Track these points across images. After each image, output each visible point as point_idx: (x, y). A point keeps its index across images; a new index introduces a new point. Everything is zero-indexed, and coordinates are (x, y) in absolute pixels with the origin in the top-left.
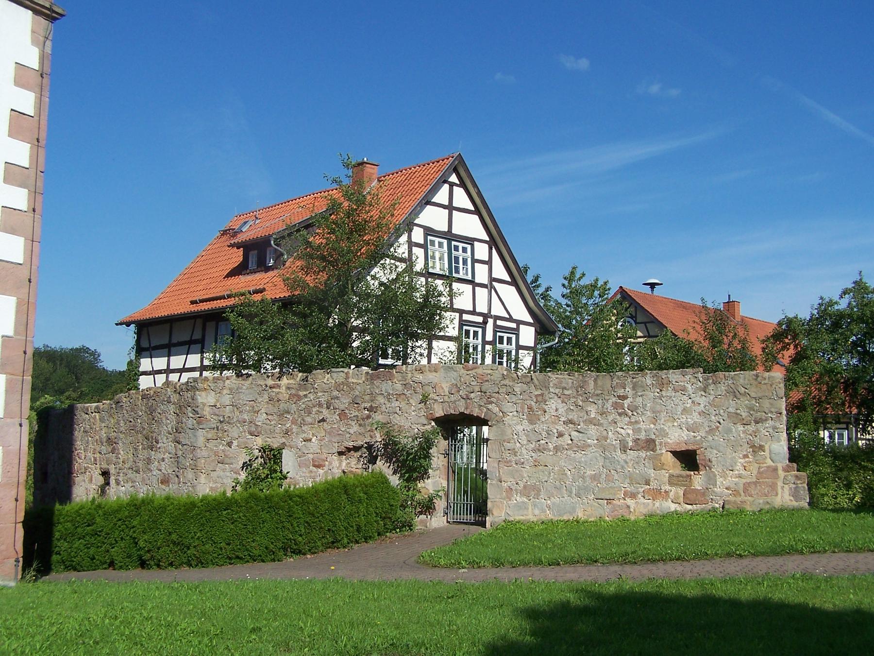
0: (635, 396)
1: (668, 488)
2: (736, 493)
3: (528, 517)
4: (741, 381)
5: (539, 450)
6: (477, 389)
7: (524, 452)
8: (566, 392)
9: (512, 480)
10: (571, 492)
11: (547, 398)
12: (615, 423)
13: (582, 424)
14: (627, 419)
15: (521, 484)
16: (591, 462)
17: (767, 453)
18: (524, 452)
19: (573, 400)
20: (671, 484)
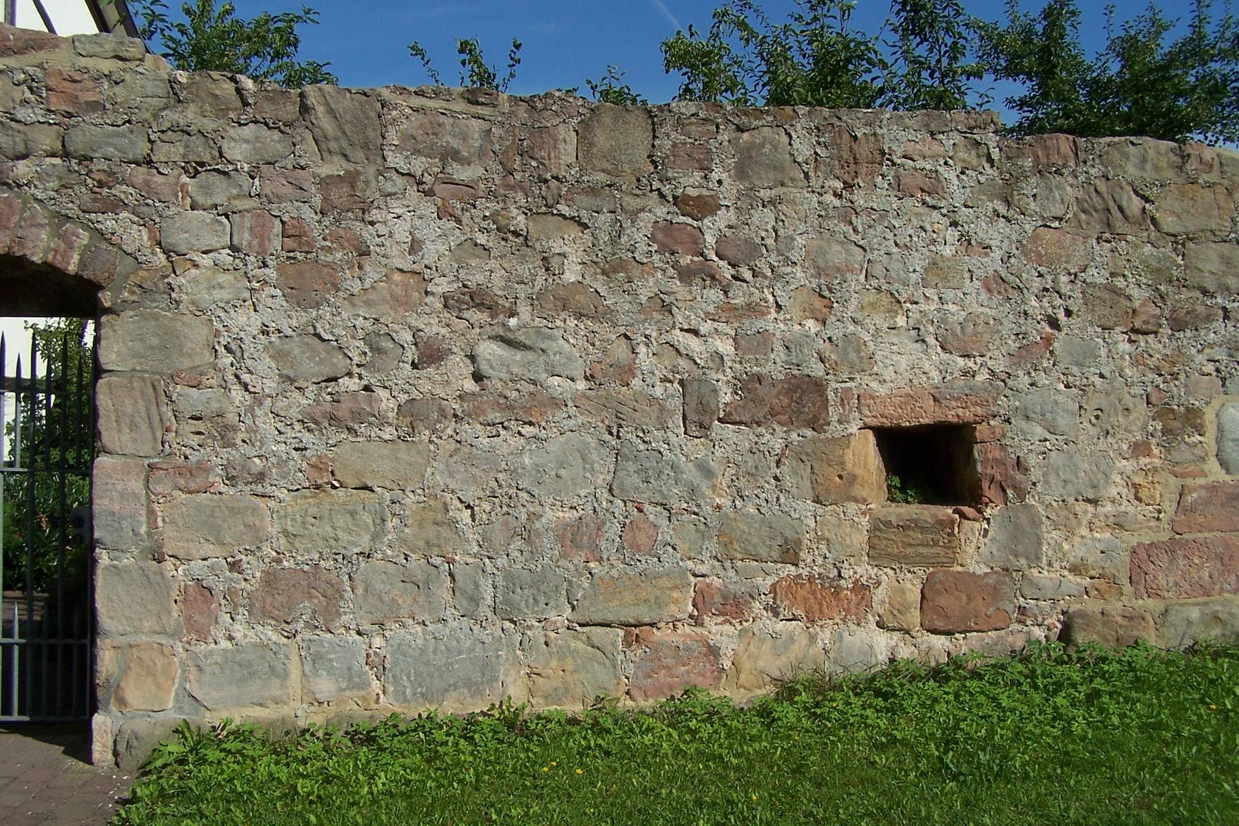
0: (748, 201)
1: (864, 570)
2: (1106, 583)
3: (285, 711)
4: (1131, 170)
5: (337, 418)
6: (46, 139)
7: (267, 425)
8: (461, 173)
9: (209, 549)
10: (475, 600)
11: (371, 194)
12: (667, 309)
13: (524, 309)
14: (714, 294)
15: (255, 569)
16: (564, 468)
17: (1209, 439)
18: (267, 425)
19: (488, 207)
20: (877, 554)
